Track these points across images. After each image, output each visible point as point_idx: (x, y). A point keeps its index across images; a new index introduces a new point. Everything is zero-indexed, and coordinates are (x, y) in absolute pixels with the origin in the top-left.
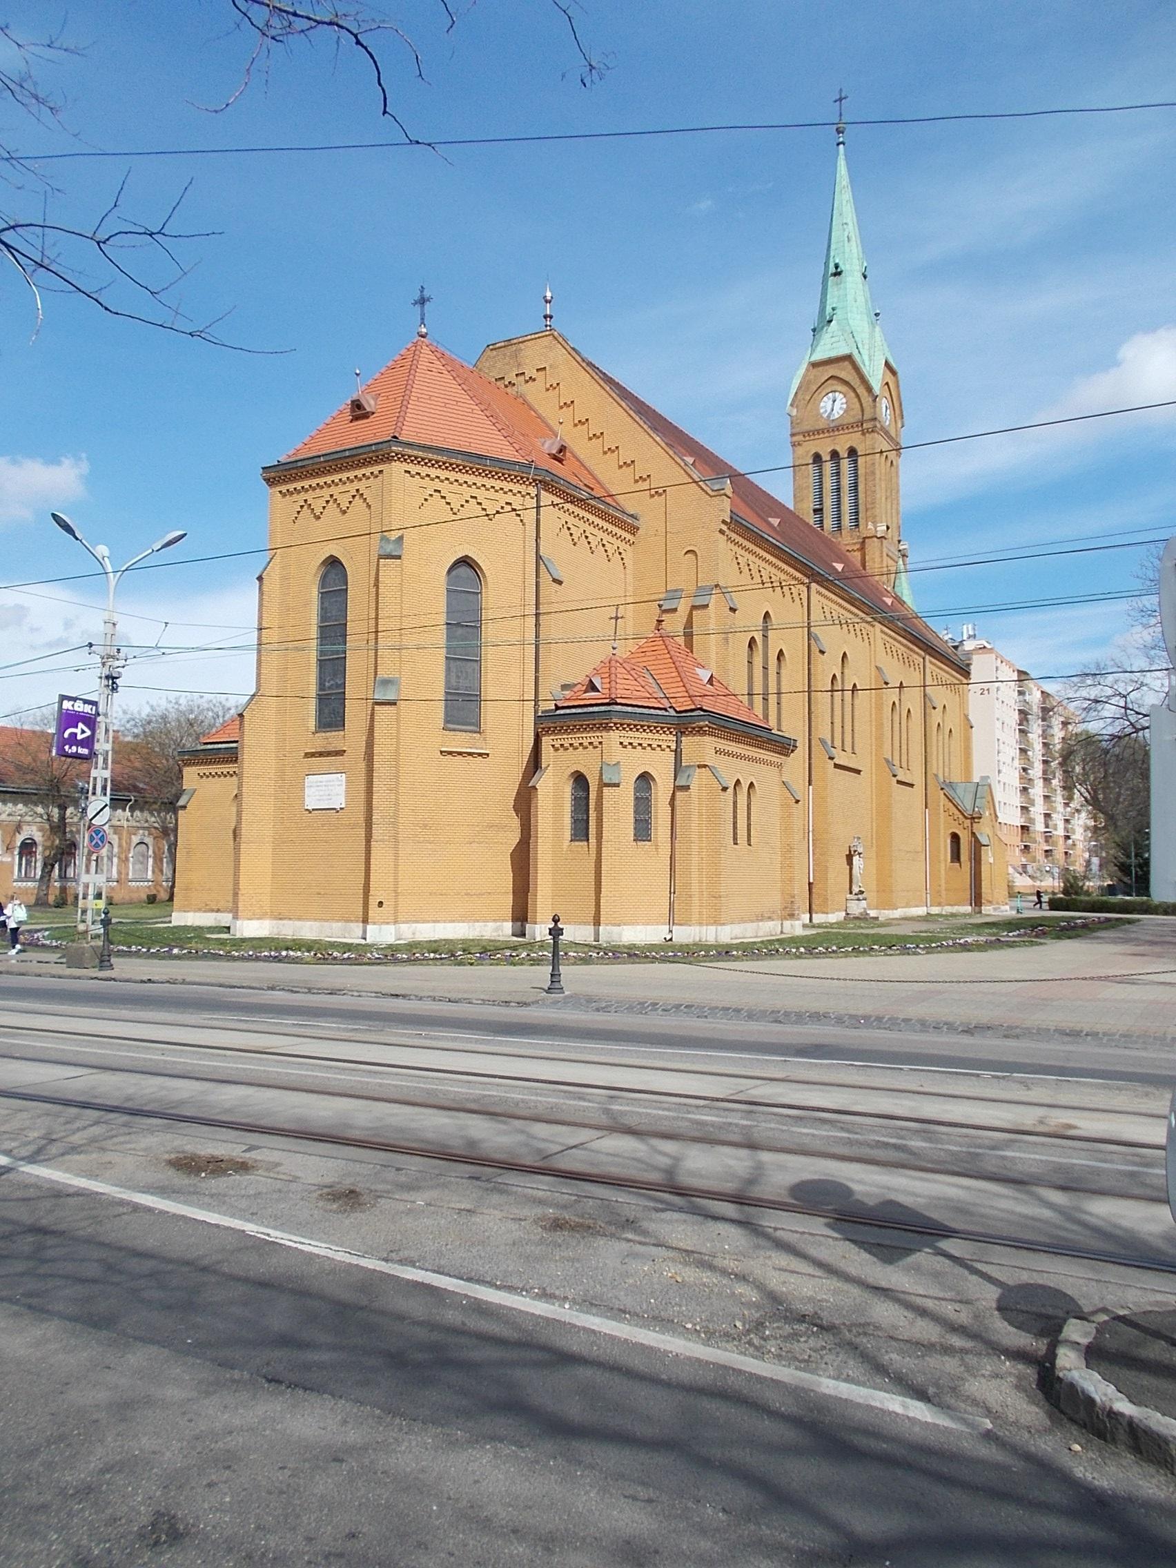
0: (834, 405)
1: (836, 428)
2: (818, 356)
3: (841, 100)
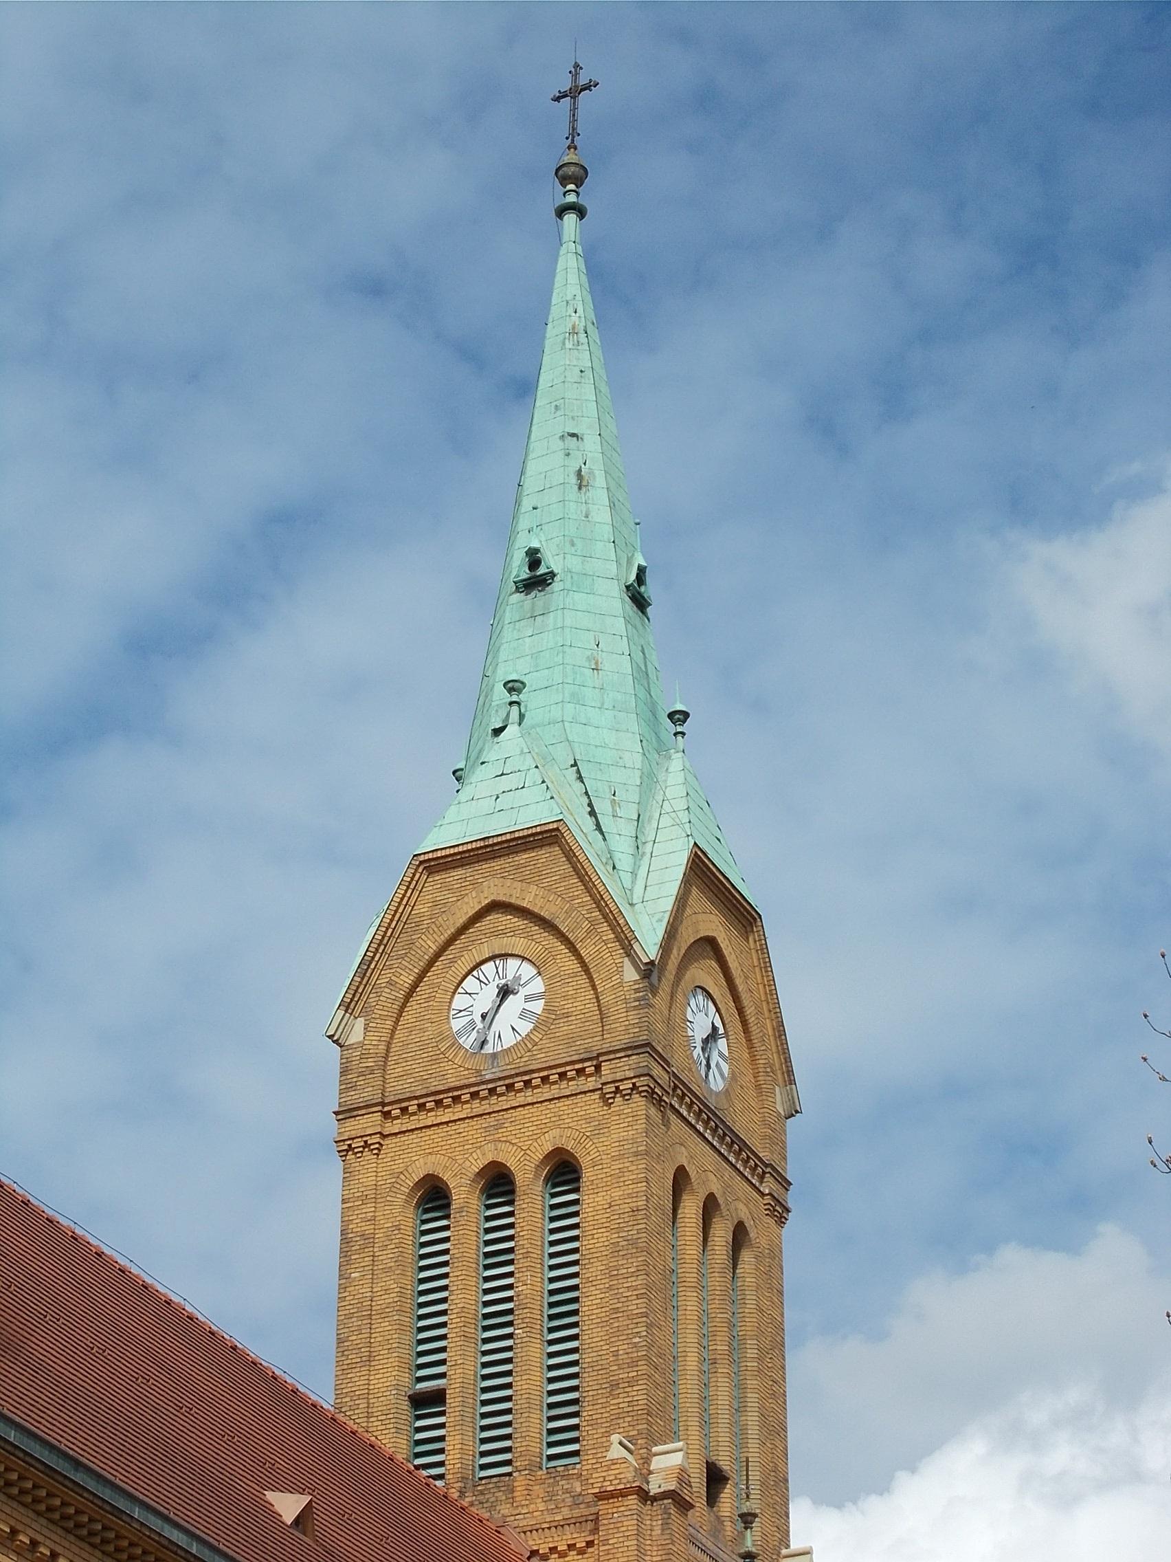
0: (500, 1006)
1: (503, 1084)
2: (447, 834)
3: (574, 92)
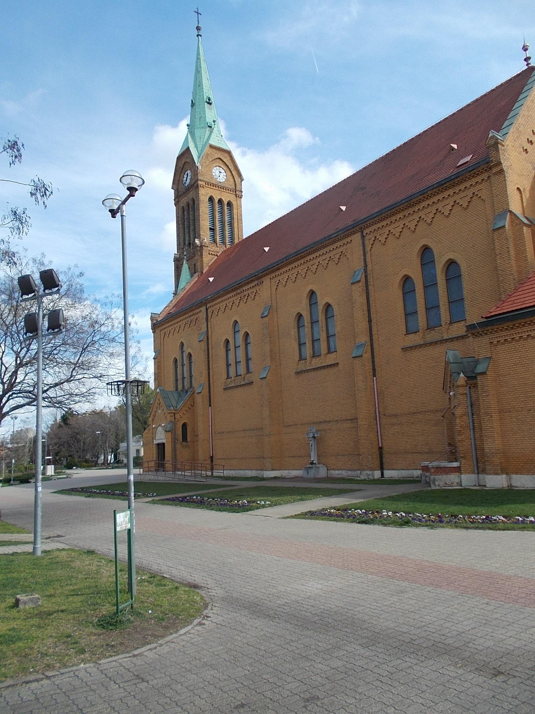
1: (220, 187)
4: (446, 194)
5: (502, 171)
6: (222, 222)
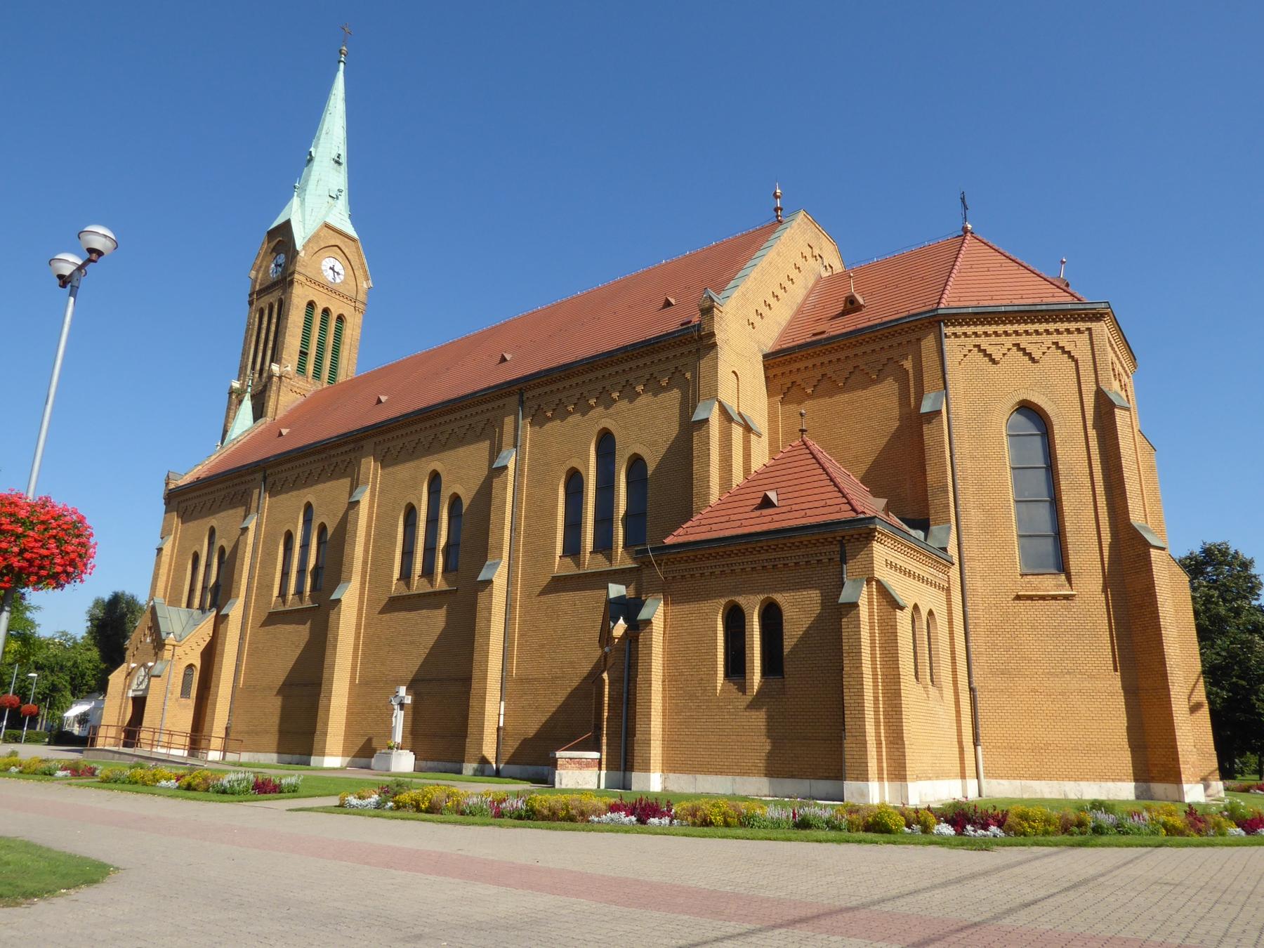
1: (330, 289)
4: (641, 362)
5: (714, 345)
6: (321, 345)
